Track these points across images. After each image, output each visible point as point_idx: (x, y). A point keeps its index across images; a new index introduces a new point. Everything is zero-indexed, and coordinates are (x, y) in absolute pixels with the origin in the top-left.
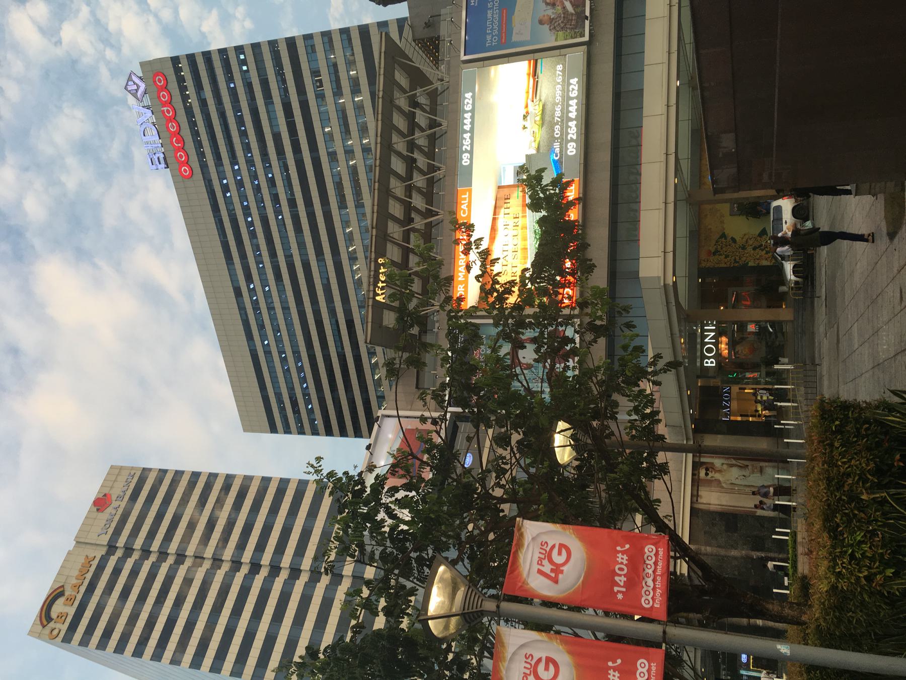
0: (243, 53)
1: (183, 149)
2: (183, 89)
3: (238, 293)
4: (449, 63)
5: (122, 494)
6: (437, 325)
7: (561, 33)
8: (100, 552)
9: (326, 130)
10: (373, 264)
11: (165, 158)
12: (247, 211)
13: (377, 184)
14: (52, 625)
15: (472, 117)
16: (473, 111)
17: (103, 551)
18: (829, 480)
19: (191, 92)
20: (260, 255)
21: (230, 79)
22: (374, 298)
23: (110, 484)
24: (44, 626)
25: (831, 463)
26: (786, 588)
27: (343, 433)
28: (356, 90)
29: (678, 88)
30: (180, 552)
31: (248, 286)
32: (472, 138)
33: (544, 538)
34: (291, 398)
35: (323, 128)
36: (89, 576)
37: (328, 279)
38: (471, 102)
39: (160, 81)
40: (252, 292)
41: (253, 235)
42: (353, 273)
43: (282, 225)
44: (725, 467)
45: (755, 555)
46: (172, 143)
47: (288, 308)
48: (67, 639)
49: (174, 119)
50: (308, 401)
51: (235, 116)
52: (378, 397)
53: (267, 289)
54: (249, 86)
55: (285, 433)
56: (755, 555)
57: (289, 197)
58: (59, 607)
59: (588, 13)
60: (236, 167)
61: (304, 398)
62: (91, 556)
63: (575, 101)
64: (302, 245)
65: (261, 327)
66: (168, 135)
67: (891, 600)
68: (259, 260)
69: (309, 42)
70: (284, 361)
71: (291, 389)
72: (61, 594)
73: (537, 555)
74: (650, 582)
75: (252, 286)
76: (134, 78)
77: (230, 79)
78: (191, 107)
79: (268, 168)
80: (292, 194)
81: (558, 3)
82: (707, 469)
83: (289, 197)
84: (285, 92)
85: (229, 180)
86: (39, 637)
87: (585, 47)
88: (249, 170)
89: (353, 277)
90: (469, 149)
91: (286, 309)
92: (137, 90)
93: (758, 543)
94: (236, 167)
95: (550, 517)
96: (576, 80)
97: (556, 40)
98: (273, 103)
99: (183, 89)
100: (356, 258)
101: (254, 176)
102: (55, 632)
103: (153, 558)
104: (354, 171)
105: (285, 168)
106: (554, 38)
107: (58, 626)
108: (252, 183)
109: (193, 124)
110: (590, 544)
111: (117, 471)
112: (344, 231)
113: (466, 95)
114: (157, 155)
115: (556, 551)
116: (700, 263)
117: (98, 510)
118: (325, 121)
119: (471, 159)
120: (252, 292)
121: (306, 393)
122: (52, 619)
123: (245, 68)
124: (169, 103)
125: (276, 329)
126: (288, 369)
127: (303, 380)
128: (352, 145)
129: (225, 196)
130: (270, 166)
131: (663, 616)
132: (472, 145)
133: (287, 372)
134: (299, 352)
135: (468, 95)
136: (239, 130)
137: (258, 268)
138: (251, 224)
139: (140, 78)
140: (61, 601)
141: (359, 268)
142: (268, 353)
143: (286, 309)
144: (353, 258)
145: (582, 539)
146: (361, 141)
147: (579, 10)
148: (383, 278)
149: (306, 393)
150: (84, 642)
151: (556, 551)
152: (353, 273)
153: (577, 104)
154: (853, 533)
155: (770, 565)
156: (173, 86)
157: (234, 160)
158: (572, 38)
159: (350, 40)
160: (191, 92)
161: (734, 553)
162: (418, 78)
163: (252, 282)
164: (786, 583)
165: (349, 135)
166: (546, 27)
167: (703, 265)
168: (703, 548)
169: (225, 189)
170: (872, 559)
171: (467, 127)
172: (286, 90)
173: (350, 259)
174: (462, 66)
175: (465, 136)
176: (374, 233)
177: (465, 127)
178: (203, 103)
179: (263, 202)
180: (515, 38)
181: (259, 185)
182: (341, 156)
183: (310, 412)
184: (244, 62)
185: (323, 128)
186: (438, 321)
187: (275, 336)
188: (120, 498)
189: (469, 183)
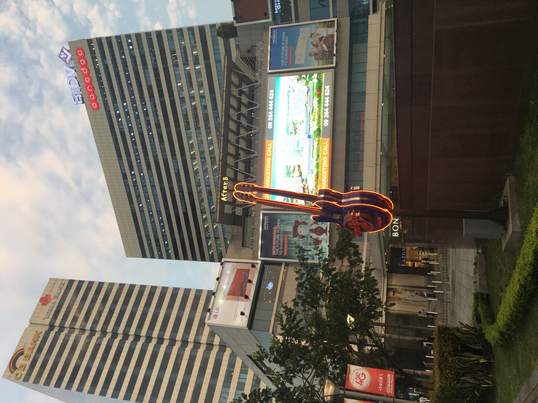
0: (131, 39)
1: (93, 93)
2: (94, 58)
3: (125, 176)
4: (261, 72)
5: (57, 295)
6: (254, 213)
7: (321, 61)
8: (45, 329)
9: (179, 84)
10: (220, 180)
11: (82, 98)
12: (131, 129)
13: (222, 138)
14: (16, 371)
16: (274, 100)
17: (46, 328)
18: (440, 353)
19: (99, 59)
20: (138, 155)
21: (122, 53)
22: (220, 199)
24: (12, 372)
25: (441, 348)
26: (432, 355)
27: (186, 258)
28: (196, 62)
29: (382, 107)
30: (82, 328)
31: (131, 173)
32: (273, 114)
33: (357, 371)
34: (155, 238)
35: (177, 84)
36: (38, 343)
37: (178, 170)
38: (273, 95)
40: (133, 176)
42: (193, 166)
43: (151, 138)
44: (403, 291)
45: (418, 339)
46: (87, 89)
47: (155, 186)
48: (26, 379)
49: (88, 75)
50: (165, 239)
51: (125, 75)
52: (206, 238)
53: (142, 174)
54: (133, 58)
55: (151, 257)
56: (418, 339)
57: (156, 122)
58: (20, 361)
59: (335, 53)
60: (125, 104)
61: (163, 238)
62: (39, 331)
63: (328, 98)
64: (163, 150)
65: (138, 196)
66: (85, 84)
67: (456, 389)
68: (137, 158)
69: (170, 34)
70: (151, 216)
71: (155, 233)
72: (22, 353)
73: (355, 377)
74: (389, 385)
75: (133, 173)
76: (65, 51)
77: (122, 53)
78: (98, 69)
79: (144, 105)
80: (158, 120)
81: (319, 45)
82: (394, 292)
83: (156, 122)
84: (155, 62)
85: (121, 111)
86: (9, 378)
87: (333, 70)
88: (133, 106)
89: (193, 169)
90: (272, 120)
91: (153, 186)
92: (66, 58)
93: (419, 333)
94: (125, 104)
95: (360, 365)
96: (329, 86)
97: (318, 65)
99: (94, 58)
100: (195, 158)
101: (135, 109)
102: (19, 376)
103: (66, 331)
104: (194, 108)
105: (154, 105)
106: (317, 63)
107: (21, 372)
108: (134, 113)
109: (99, 79)
110: (371, 373)
111: (54, 282)
113: (270, 91)
114: (77, 96)
115: (361, 375)
116: (391, 184)
117: (43, 304)
118: (178, 79)
119: (273, 125)
120: (133, 176)
121: (164, 235)
122: (16, 368)
123: (131, 47)
124: (85, 66)
125: (147, 198)
126: (154, 221)
127: (163, 227)
128: (194, 94)
129: (118, 121)
130: (145, 104)
131: (393, 396)
132: (273, 117)
133: (153, 223)
134: (160, 211)
135: (272, 91)
136: (127, 83)
137: (137, 162)
138: (133, 137)
140: (22, 357)
141: (196, 164)
142: (142, 211)
143: (153, 186)
144: (193, 158)
145: (369, 372)
146: (199, 92)
147: (330, 49)
148: (225, 188)
149: (164, 235)
150: (37, 381)
151: (361, 375)
152: (193, 166)
153: (329, 99)
154: (446, 370)
155: (425, 344)
156: (88, 56)
158: (327, 64)
159: (193, 34)
160: (99, 59)
161: (408, 338)
162: (244, 79)
163: (133, 170)
164: (432, 353)
165: (195, 92)
166: (313, 57)
167: (393, 185)
168: (392, 335)
169: (118, 116)
170: (451, 378)
171: (271, 108)
172: (155, 61)
173: (191, 158)
175: (269, 113)
176: (221, 164)
177: (270, 108)
178: (106, 67)
179: (140, 124)
180: (297, 62)
181: (138, 114)
182: (187, 100)
183: (167, 246)
184: (131, 44)
185: (177, 84)
186: (254, 211)
187: (146, 202)
189: (271, 138)
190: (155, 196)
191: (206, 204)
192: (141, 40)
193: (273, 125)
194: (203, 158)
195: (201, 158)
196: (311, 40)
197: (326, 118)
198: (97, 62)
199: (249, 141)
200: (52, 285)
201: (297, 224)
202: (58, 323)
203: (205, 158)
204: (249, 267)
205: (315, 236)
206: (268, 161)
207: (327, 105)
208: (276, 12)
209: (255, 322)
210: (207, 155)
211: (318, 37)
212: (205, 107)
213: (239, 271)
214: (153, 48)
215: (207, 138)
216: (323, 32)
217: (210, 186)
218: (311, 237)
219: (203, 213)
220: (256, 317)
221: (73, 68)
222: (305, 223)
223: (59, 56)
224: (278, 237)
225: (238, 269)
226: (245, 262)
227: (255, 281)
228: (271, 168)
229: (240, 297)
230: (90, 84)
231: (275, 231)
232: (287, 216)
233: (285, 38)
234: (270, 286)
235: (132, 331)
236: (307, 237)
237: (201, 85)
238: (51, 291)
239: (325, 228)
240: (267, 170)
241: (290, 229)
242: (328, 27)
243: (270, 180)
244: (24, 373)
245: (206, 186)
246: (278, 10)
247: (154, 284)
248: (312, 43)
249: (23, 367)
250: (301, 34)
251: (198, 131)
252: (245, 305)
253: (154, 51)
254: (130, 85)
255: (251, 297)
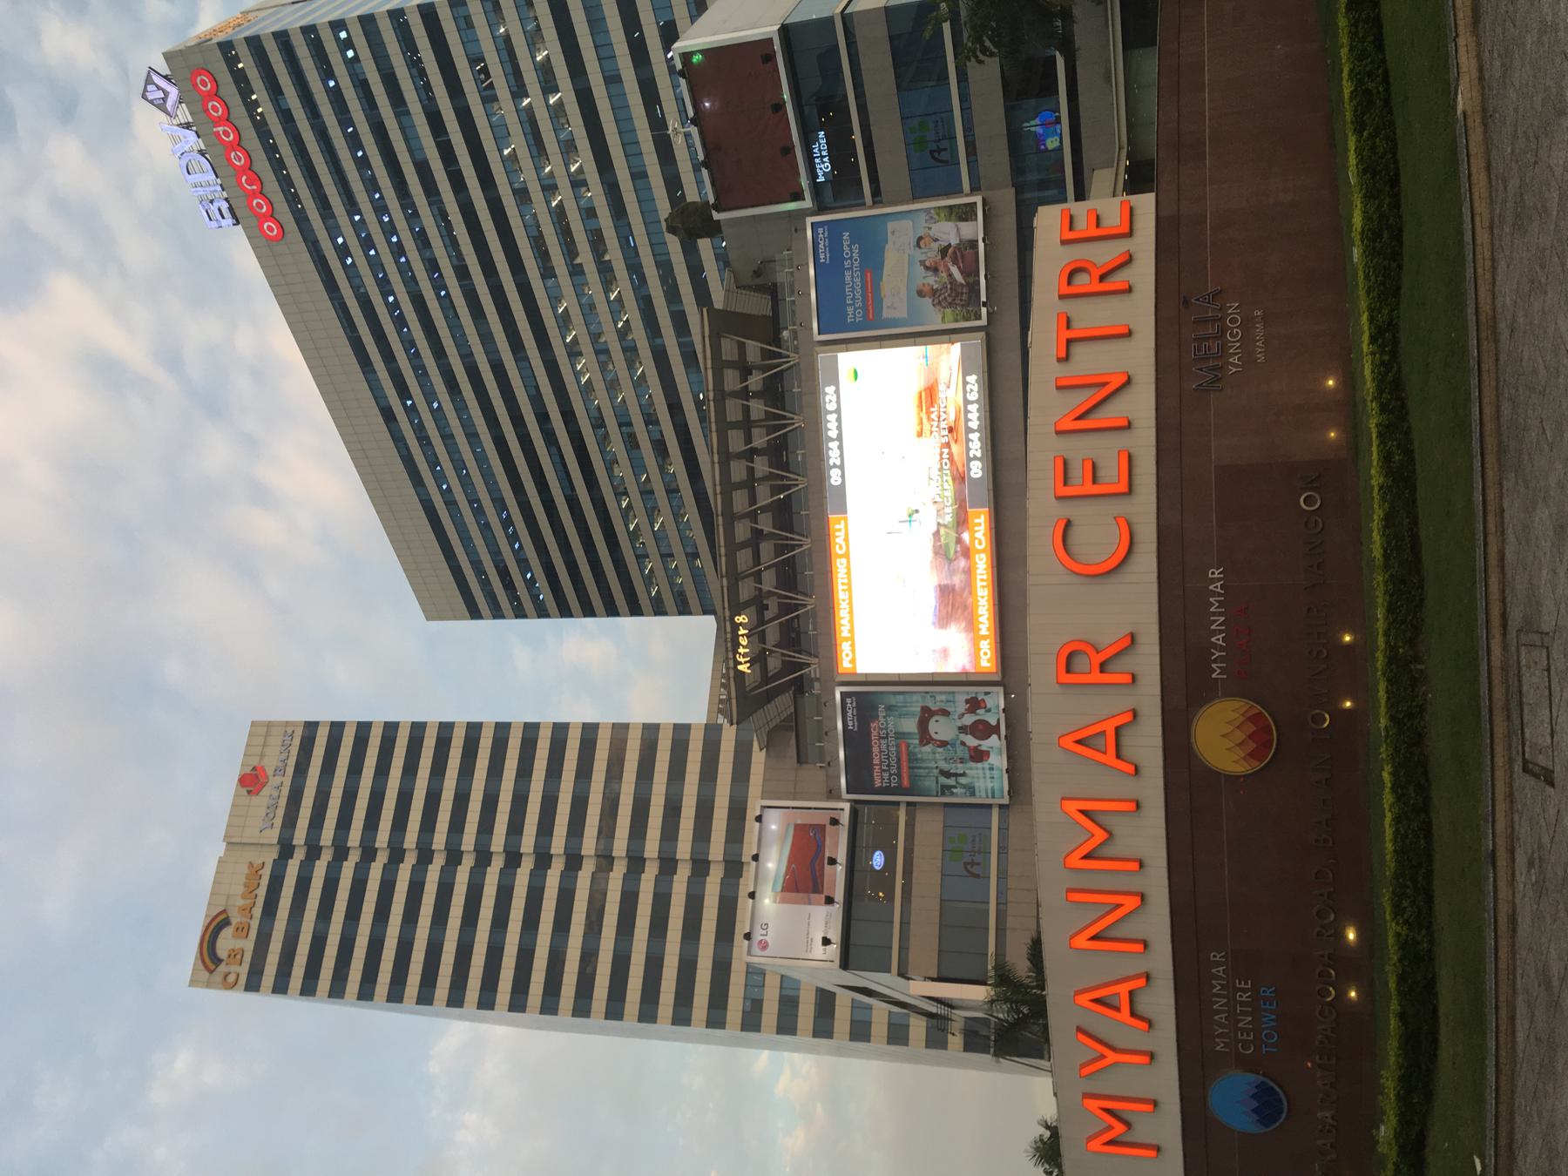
6: (817, 685)
7: (948, 311)
11: (231, 209)
12: (385, 286)
14: (222, 968)
15: (839, 420)
17: (274, 854)
19: (259, 94)
21: (327, 72)
23: (258, 750)
24: (211, 972)
28: (549, 86)
31: (404, 405)
32: (841, 447)
36: (262, 892)
37: (537, 388)
38: (834, 398)
39: (204, 83)
40: (412, 411)
41: (400, 322)
42: (577, 375)
43: (447, 304)
49: (238, 144)
52: (637, 557)
54: (363, 86)
57: (455, 262)
58: (226, 942)
64: (486, 338)
65: (433, 462)
66: (232, 172)
70: (479, 512)
71: (496, 553)
76: (156, 79)
77: (327, 72)
80: (460, 256)
84: (425, 90)
85: (347, 237)
86: (208, 985)
87: (983, 334)
89: (578, 382)
91: (472, 436)
92: (164, 100)
98: (408, 113)
102: (231, 978)
104: (559, 214)
105: (442, 215)
107: (234, 968)
109: (271, 150)
111: (263, 730)
112: (554, 309)
114: (216, 204)
119: (843, 476)
120: (412, 411)
122: (221, 961)
125: (459, 465)
127: (513, 538)
132: (842, 456)
133: (486, 528)
134: (423, 367)
135: (830, 390)
136: (355, 158)
138: (396, 305)
139: (166, 77)
140: (227, 933)
142: (451, 504)
143: (472, 436)
144: (574, 352)
147: (971, 280)
148: (744, 641)
152: (577, 375)
156: (229, 89)
157: (352, 206)
166: (928, 301)
169: (343, 251)
171: (833, 434)
172: (428, 87)
174: (818, 349)
177: (830, 434)
178: (286, 117)
180: (887, 314)
182: (536, 194)
184: (348, 43)
188: (280, 771)
189: (842, 509)
190: (481, 459)
191: (623, 470)
192: (378, 33)
193: (843, 476)
194: (602, 352)
195: (597, 352)
196: (919, 255)
197: (975, 458)
198: (256, 104)
199: (785, 514)
200: (261, 740)
201: (926, 715)
202: (300, 836)
203: (607, 352)
204: (823, 818)
205: (971, 741)
206: (839, 566)
207: (974, 424)
208: (821, 179)
209: (852, 951)
210: (611, 339)
211: (935, 246)
212: (589, 213)
213: (801, 830)
214: (415, 51)
215: (607, 298)
216: (949, 232)
217: (630, 424)
218: (963, 743)
219: (620, 493)
220: (853, 940)
221: (187, 126)
222: (945, 713)
223: (144, 97)
224: (884, 747)
225: (797, 827)
226: (815, 809)
227: (842, 857)
228: (849, 584)
229: (813, 896)
230: (249, 167)
231: (874, 733)
232: (900, 698)
233: (851, 251)
234: (878, 860)
235: (498, 842)
236: (953, 745)
237: (568, 148)
238: (262, 756)
239: (993, 723)
240: (840, 587)
241: (910, 725)
242: (962, 219)
243: (851, 613)
244: (244, 970)
245: (620, 425)
246: (825, 174)
247: (532, 718)
248: (922, 263)
249: (235, 955)
250: (890, 236)
251: (578, 279)
252: (829, 915)
253: (419, 59)
254: (363, 164)
255: (839, 895)
